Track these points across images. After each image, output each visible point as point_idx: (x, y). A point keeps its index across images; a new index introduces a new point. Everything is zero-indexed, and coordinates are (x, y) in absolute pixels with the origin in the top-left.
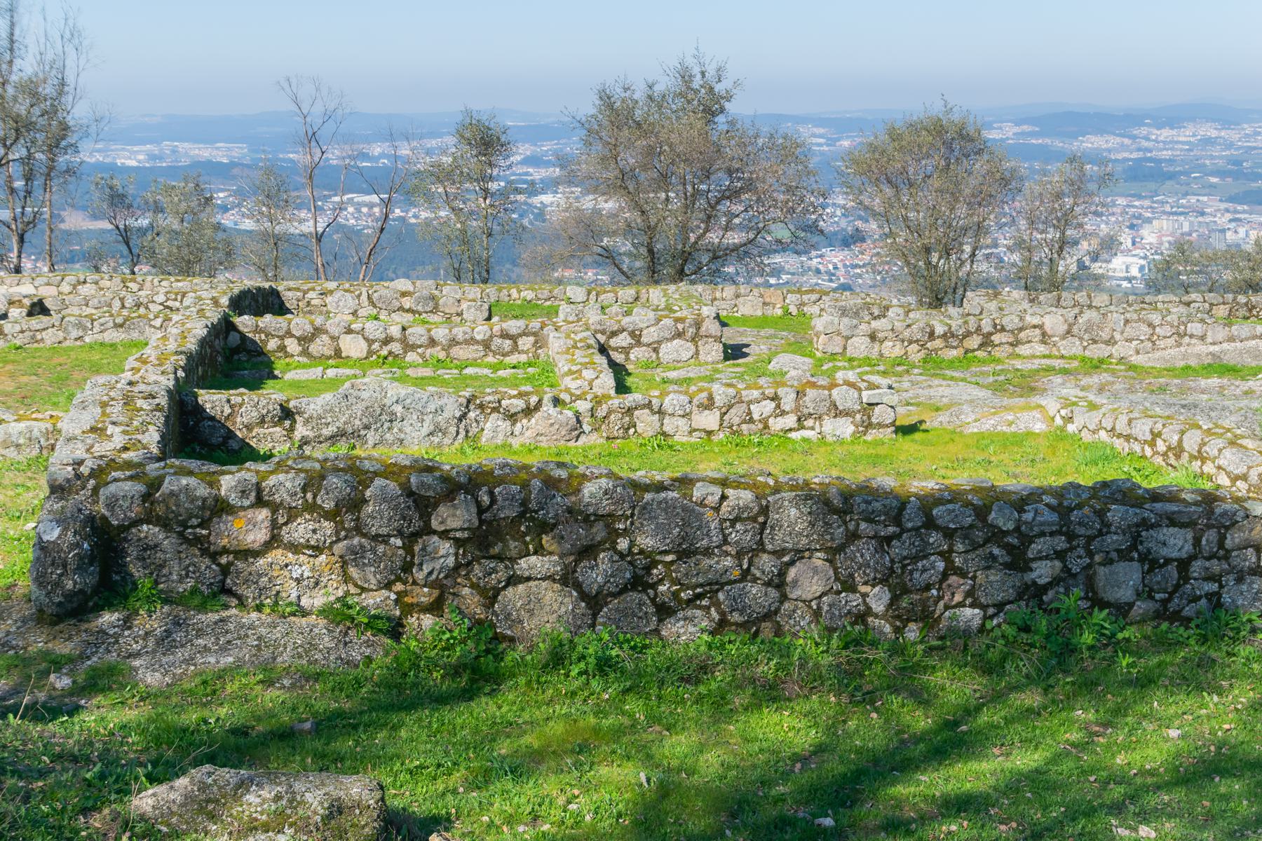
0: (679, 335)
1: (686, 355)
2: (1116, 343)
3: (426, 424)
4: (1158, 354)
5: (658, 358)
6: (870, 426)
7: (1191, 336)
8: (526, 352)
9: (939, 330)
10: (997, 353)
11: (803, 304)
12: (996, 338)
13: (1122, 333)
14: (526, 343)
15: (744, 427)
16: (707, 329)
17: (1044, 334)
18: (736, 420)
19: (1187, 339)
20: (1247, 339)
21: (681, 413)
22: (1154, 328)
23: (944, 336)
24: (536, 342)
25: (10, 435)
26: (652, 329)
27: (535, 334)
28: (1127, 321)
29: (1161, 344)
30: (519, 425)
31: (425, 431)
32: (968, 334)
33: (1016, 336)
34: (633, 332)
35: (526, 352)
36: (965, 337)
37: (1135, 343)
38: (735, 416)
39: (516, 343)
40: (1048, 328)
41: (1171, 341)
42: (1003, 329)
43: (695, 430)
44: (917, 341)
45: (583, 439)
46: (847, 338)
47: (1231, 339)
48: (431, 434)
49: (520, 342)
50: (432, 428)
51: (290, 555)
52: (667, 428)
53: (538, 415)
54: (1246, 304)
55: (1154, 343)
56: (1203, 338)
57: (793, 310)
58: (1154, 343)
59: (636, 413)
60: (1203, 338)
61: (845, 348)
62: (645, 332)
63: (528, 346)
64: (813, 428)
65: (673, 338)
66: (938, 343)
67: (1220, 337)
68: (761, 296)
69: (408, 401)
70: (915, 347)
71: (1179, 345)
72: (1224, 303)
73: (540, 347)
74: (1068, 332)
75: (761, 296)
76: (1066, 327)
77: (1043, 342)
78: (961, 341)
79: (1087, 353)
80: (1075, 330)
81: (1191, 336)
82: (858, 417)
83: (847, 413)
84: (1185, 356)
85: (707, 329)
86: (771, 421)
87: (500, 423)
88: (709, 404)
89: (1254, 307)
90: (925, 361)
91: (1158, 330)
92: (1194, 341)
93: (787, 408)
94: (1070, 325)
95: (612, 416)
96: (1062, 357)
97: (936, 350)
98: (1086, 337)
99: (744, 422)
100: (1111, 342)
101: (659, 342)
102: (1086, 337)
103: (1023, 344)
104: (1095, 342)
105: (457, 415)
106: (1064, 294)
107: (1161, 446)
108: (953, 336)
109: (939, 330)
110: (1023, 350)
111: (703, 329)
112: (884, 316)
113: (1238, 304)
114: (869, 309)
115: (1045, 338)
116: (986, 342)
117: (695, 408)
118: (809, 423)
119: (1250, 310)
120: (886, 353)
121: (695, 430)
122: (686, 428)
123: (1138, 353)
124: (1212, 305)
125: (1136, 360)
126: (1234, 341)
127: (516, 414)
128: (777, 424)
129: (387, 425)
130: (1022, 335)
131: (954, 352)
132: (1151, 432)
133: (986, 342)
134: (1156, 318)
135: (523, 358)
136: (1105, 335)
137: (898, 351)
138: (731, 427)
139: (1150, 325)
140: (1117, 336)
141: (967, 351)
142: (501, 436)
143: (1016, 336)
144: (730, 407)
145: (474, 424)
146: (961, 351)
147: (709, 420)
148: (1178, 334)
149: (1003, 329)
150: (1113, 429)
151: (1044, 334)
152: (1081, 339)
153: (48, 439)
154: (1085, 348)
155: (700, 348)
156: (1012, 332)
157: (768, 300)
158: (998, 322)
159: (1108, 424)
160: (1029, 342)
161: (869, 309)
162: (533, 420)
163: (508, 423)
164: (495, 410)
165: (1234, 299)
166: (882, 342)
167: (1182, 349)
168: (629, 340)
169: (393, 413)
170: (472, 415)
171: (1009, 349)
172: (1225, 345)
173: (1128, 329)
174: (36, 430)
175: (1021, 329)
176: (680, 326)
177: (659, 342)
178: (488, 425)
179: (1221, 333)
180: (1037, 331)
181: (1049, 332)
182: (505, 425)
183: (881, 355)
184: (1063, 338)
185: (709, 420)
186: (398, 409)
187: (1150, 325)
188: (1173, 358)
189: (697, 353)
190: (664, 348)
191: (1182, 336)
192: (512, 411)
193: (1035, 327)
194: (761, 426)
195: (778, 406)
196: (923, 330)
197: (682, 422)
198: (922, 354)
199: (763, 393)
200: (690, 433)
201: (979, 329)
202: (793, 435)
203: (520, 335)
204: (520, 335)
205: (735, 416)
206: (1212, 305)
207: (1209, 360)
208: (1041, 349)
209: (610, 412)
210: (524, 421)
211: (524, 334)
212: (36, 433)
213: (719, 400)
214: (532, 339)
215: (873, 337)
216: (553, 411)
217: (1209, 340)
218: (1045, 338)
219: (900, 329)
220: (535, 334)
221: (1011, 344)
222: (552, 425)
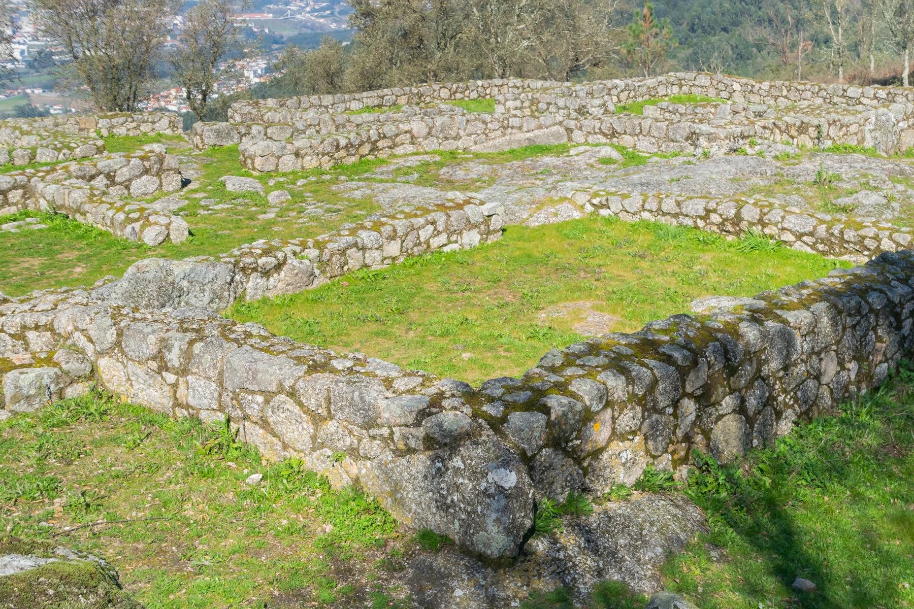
0: (146, 171)
1: (152, 188)
2: (461, 138)
3: (207, 294)
4: (491, 143)
5: (129, 194)
6: (489, 233)
7: (512, 128)
8: (16, 204)
9: (343, 142)
10: (382, 155)
11: (113, 127)
12: (380, 144)
13: (465, 130)
14: (15, 196)
15: (415, 249)
16: (169, 163)
17: (412, 137)
18: (411, 245)
19: (509, 130)
20: (550, 126)
21: (376, 246)
22: (487, 124)
23: (346, 147)
24: (25, 194)
25: (21, 388)
26: (125, 169)
27: (23, 187)
28: (468, 121)
29: (492, 135)
30: (271, 279)
31: (206, 300)
32: (362, 144)
33: (393, 141)
34: (109, 174)
35: (16, 204)
36: (360, 145)
37: (473, 136)
38: (409, 243)
39: (6, 196)
40: (415, 132)
41: (499, 133)
42: (385, 137)
43: (385, 258)
44: (328, 154)
45: (316, 282)
46: (279, 158)
47: (540, 127)
48: (211, 301)
49: (10, 196)
50: (212, 296)
51: (621, 444)
52: (368, 261)
53: (285, 268)
54: (417, 94)
55: (487, 135)
56: (520, 128)
57: (105, 132)
58: (487, 135)
59: (348, 252)
60: (520, 128)
61: (277, 166)
62: (119, 172)
63: (18, 198)
64: (456, 242)
65: (142, 175)
66: (342, 153)
67: (532, 126)
68: (77, 123)
69: (192, 275)
70: (327, 158)
71: (504, 135)
72: (404, 95)
73: (29, 198)
74: (429, 134)
75: (77, 123)
76: (427, 130)
77: (412, 143)
78: (357, 149)
79: (442, 148)
80: (434, 132)
81: (512, 128)
82: (482, 227)
83: (476, 226)
84: (510, 143)
85: (169, 163)
86: (431, 241)
87: (259, 281)
88: (392, 238)
89: (422, 95)
90: (334, 167)
91: (489, 125)
92: (514, 131)
93: (440, 229)
94: (430, 128)
95: (334, 258)
96: (427, 153)
97: (341, 159)
98: (441, 136)
99: (416, 245)
100: (457, 138)
101: (130, 180)
102: (441, 136)
103: (398, 146)
104: (447, 139)
105: (229, 280)
106: (302, 98)
107: (715, 218)
108: (352, 146)
109: (343, 142)
110: (399, 151)
111: (165, 164)
112: (249, 134)
113: (413, 94)
114: (237, 129)
115: (413, 140)
116: (374, 149)
117: (385, 241)
118: (454, 238)
119: (420, 98)
120: (306, 166)
121: (385, 258)
122: (380, 258)
123: (476, 143)
124: (397, 96)
125: (474, 148)
126: (542, 128)
127: (269, 271)
128: (435, 243)
129: (177, 300)
130: (398, 139)
131: (353, 159)
132: (705, 209)
133: (374, 149)
134: (487, 117)
135: (13, 209)
136: (453, 133)
137: (315, 163)
138: (407, 252)
139: (484, 122)
140: (462, 133)
141: (362, 156)
142: (260, 292)
143: (393, 141)
144: (407, 235)
145: (240, 286)
146: (358, 156)
147: (393, 249)
148: (503, 127)
149: (385, 137)
150: (659, 209)
151: (412, 137)
152: (438, 138)
153: (57, 384)
154: (440, 144)
155: (164, 180)
156: (390, 138)
157: (83, 126)
158: (381, 131)
159: (652, 205)
160: (403, 144)
161: (237, 129)
162: (283, 273)
163: (265, 279)
164: (255, 270)
165: (411, 91)
166: (303, 158)
167: (507, 137)
168: (105, 181)
169: (181, 289)
170: (237, 278)
171: (388, 151)
172: (536, 132)
173: (469, 127)
174: (45, 377)
175: (397, 135)
176: (147, 164)
177: (130, 180)
178: (250, 284)
179: (533, 123)
180: (408, 135)
181: (416, 135)
182: (262, 282)
183: (303, 168)
184: (426, 138)
185: (393, 249)
186: (185, 284)
187: (484, 122)
188: (502, 144)
189: (161, 185)
190: (135, 184)
191: (505, 128)
192: (268, 268)
193: (406, 132)
194: (425, 246)
195: (435, 229)
196: (331, 144)
197: (377, 254)
198: (331, 164)
199: (427, 220)
200: (382, 261)
201: (369, 138)
202: (445, 249)
203: (10, 189)
204: (10, 189)
205: (409, 243)
206: (397, 96)
207: (526, 144)
208: (410, 149)
209: (332, 255)
210: (275, 275)
211: (14, 188)
212: (46, 380)
213: (400, 231)
214: (20, 191)
215: (297, 155)
216: (296, 262)
217: (525, 129)
218: (413, 140)
219: (316, 145)
220: (23, 187)
221: (390, 148)
222: (297, 274)
